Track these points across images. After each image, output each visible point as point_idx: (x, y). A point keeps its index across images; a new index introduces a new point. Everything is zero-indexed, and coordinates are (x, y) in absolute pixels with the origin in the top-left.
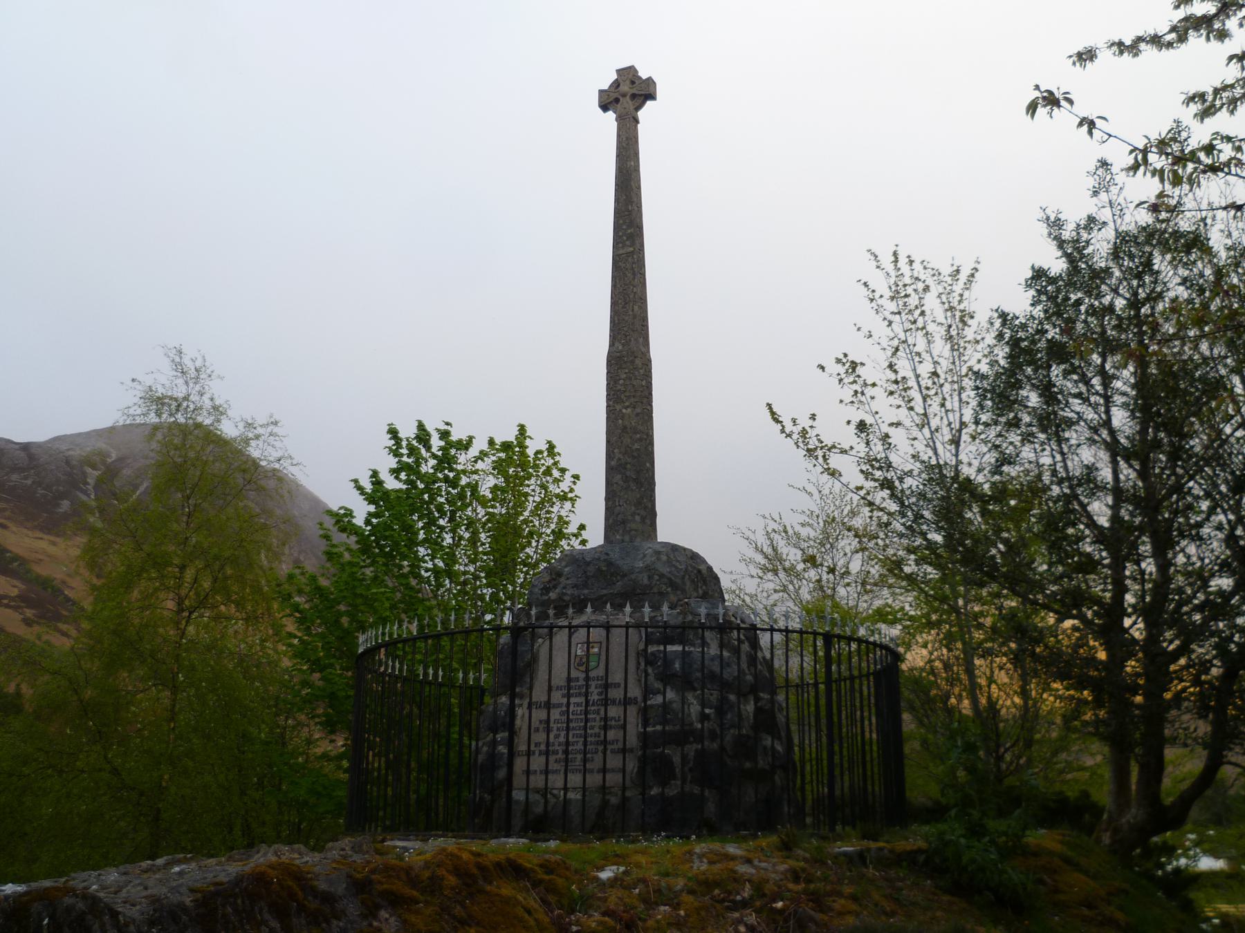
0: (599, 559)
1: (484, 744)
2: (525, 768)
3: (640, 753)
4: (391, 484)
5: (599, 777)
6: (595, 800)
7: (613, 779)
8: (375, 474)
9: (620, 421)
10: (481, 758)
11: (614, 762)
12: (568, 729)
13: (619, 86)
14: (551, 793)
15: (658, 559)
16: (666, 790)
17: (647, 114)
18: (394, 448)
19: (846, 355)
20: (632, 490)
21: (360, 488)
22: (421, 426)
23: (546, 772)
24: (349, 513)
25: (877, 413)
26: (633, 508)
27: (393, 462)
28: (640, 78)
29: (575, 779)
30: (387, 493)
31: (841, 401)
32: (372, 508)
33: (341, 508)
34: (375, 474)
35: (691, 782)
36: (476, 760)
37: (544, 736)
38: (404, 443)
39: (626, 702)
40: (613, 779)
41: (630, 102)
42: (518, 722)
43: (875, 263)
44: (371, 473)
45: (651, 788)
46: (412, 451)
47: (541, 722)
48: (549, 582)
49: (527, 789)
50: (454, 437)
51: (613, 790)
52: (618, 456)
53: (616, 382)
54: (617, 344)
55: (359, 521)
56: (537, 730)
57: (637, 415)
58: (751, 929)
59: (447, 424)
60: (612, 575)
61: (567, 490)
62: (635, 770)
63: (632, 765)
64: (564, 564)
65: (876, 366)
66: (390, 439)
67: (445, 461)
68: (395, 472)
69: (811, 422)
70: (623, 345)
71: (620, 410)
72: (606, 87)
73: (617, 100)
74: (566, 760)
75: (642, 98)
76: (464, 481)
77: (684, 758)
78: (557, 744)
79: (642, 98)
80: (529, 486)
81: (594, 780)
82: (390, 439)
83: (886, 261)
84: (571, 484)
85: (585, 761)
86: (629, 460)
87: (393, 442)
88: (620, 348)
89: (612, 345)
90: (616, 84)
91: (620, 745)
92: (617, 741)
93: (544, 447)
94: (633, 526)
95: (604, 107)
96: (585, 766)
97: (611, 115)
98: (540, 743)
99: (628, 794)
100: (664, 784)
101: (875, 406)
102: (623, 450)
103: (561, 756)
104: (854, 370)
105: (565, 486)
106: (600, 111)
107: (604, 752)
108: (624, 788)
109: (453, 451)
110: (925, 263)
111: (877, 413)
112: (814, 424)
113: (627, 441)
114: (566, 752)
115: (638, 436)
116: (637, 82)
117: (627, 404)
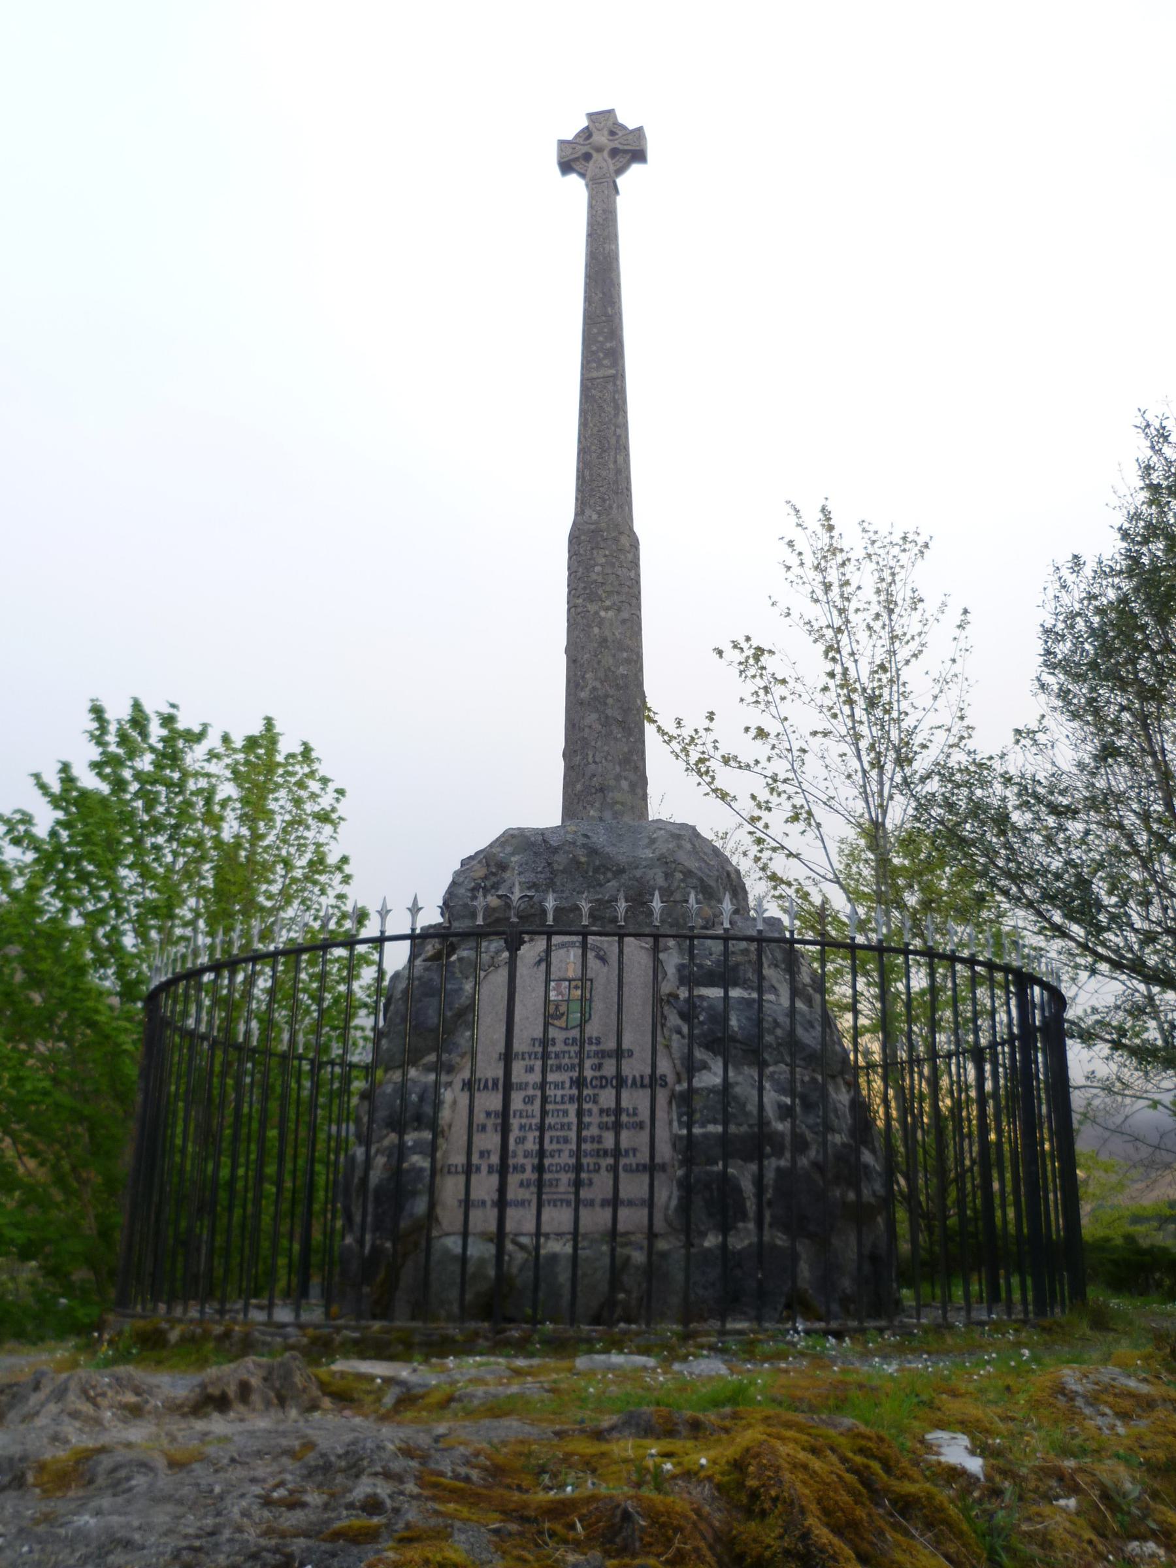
0: (574, 843)
1: (378, 1151)
2: (462, 1196)
3: (680, 1173)
4: (89, 781)
5: (606, 1215)
6: (597, 1255)
7: (631, 1219)
8: (65, 768)
9: (596, 630)
10: (375, 1177)
11: (633, 1187)
12: (542, 1128)
13: (590, 136)
14: (515, 1243)
15: (679, 847)
16: (731, 1240)
17: (631, 181)
18: (97, 733)
19: (748, 639)
20: (616, 739)
21: (43, 787)
22: (137, 706)
23: (615, 1202)
24: (27, 819)
25: (786, 719)
26: (618, 769)
27: (95, 753)
28: (624, 127)
29: (558, 1218)
30: (84, 794)
31: (742, 700)
32: (60, 815)
33: (16, 811)
34: (65, 768)
35: (771, 1225)
36: (365, 1180)
37: (496, 1139)
38: (113, 728)
39: (654, 1082)
40: (631, 1219)
41: (609, 160)
42: (445, 1114)
43: (794, 520)
44: (60, 766)
45: (703, 1235)
46: (123, 739)
47: (488, 1114)
48: (486, 878)
49: (465, 1235)
50: (181, 725)
51: (633, 1238)
52: (592, 683)
53: (589, 569)
54: (588, 512)
55: (41, 830)
56: (483, 1128)
57: (624, 622)
58: (2, 1284)
59: (173, 706)
60: (596, 870)
61: (329, 808)
62: (674, 1202)
63: (667, 1195)
64: (509, 849)
65: (785, 658)
66: (93, 720)
67: (170, 756)
68: (96, 766)
69: (707, 723)
70: (599, 514)
71: (596, 613)
72: (569, 136)
73: (587, 157)
74: (540, 1184)
75: (628, 157)
76: (191, 785)
77: (759, 1181)
78: (520, 1153)
79: (628, 157)
80: (276, 800)
81: (596, 1219)
82: (93, 720)
83: (812, 519)
84: (333, 802)
85: (578, 1184)
86: (612, 692)
87: (96, 725)
88: (595, 517)
89: (580, 512)
90: (586, 133)
91: (643, 1157)
92: (635, 1150)
93: (298, 749)
94: (618, 796)
95: (566, 167)
96: (577, 1194)
97: (574, 180)
98: (489, 1152)
99: (662, 1245)
100: (725, 1229)
101: (785, 709)
102: (601, 674)
103: (530, 1175)
104: (757, 658)
105: (326, 802)
106: (557, 170)
107: (614, 1169)
108: (652, 1235)
109: (180, 744)
110: (865, 525)
111: (786, 719)
112: (712, 726)
113: (608, 661)
114: (540, 1169)
115: (625, 655)
116: (620, 133)
117: (608, 603)
